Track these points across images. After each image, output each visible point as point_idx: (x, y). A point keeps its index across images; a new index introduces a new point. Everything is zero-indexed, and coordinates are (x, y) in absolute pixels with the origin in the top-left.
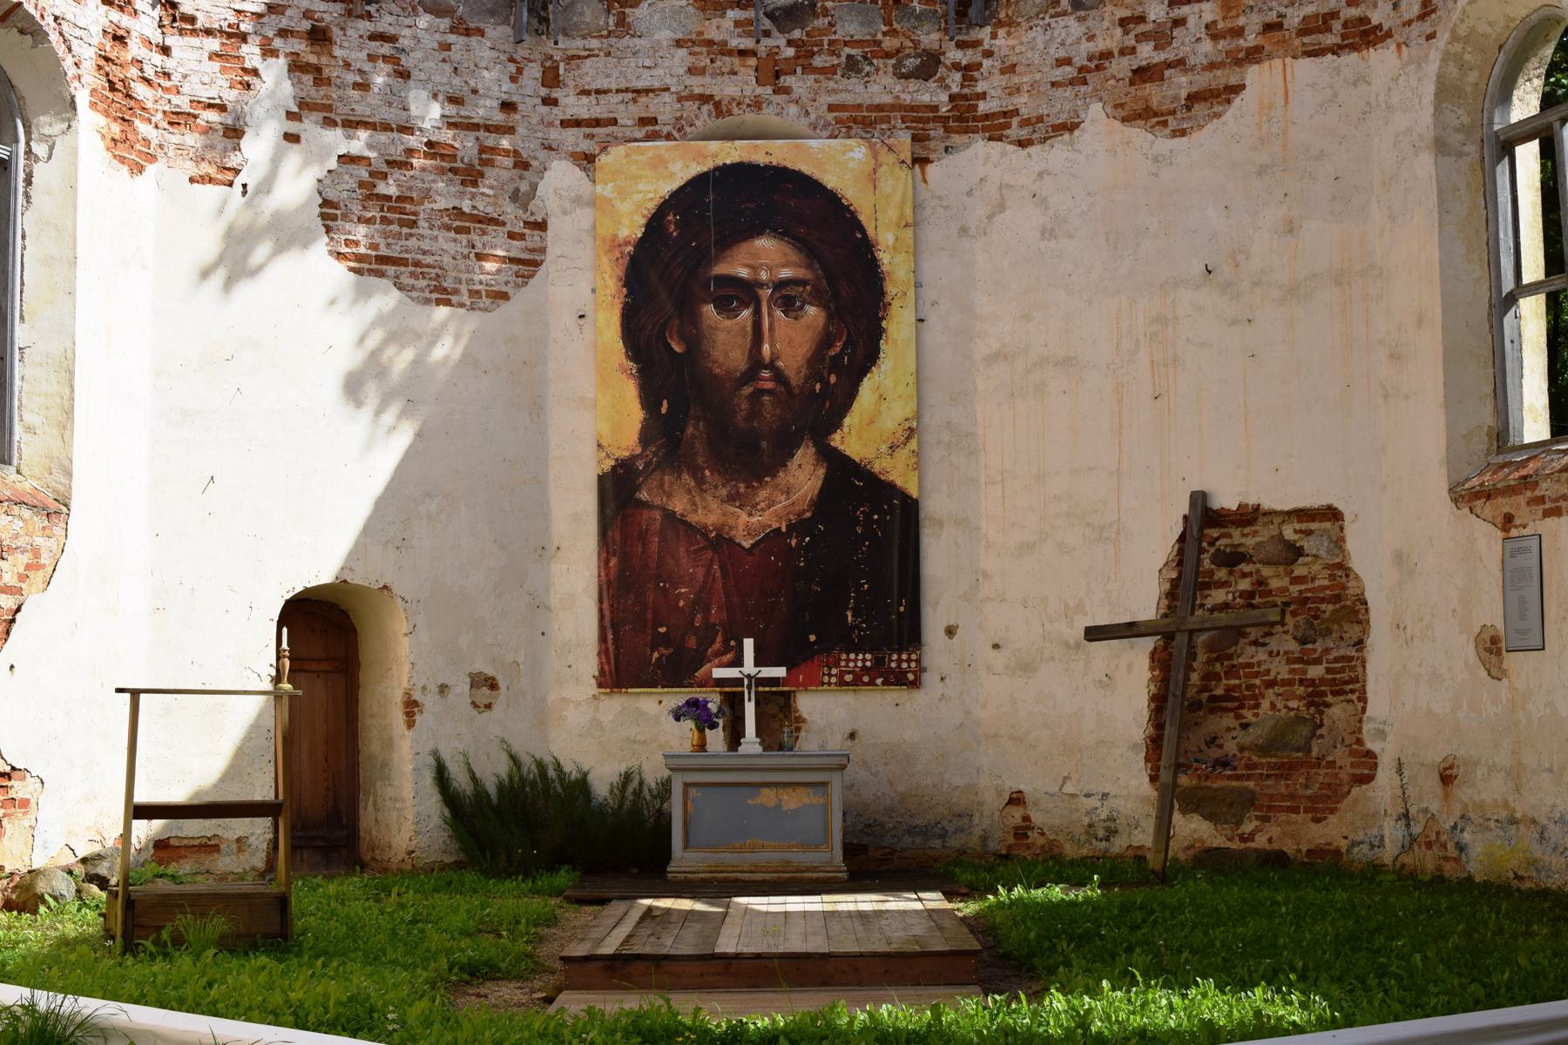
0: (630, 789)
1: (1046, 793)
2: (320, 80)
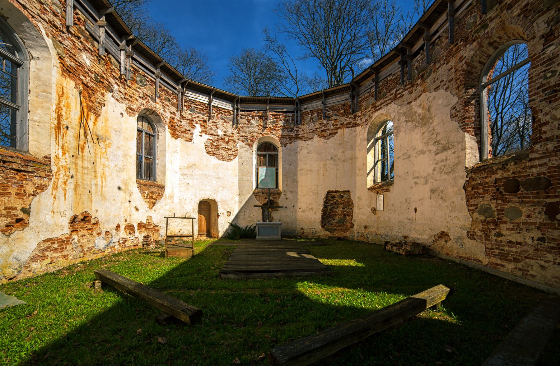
0: (248, 228)
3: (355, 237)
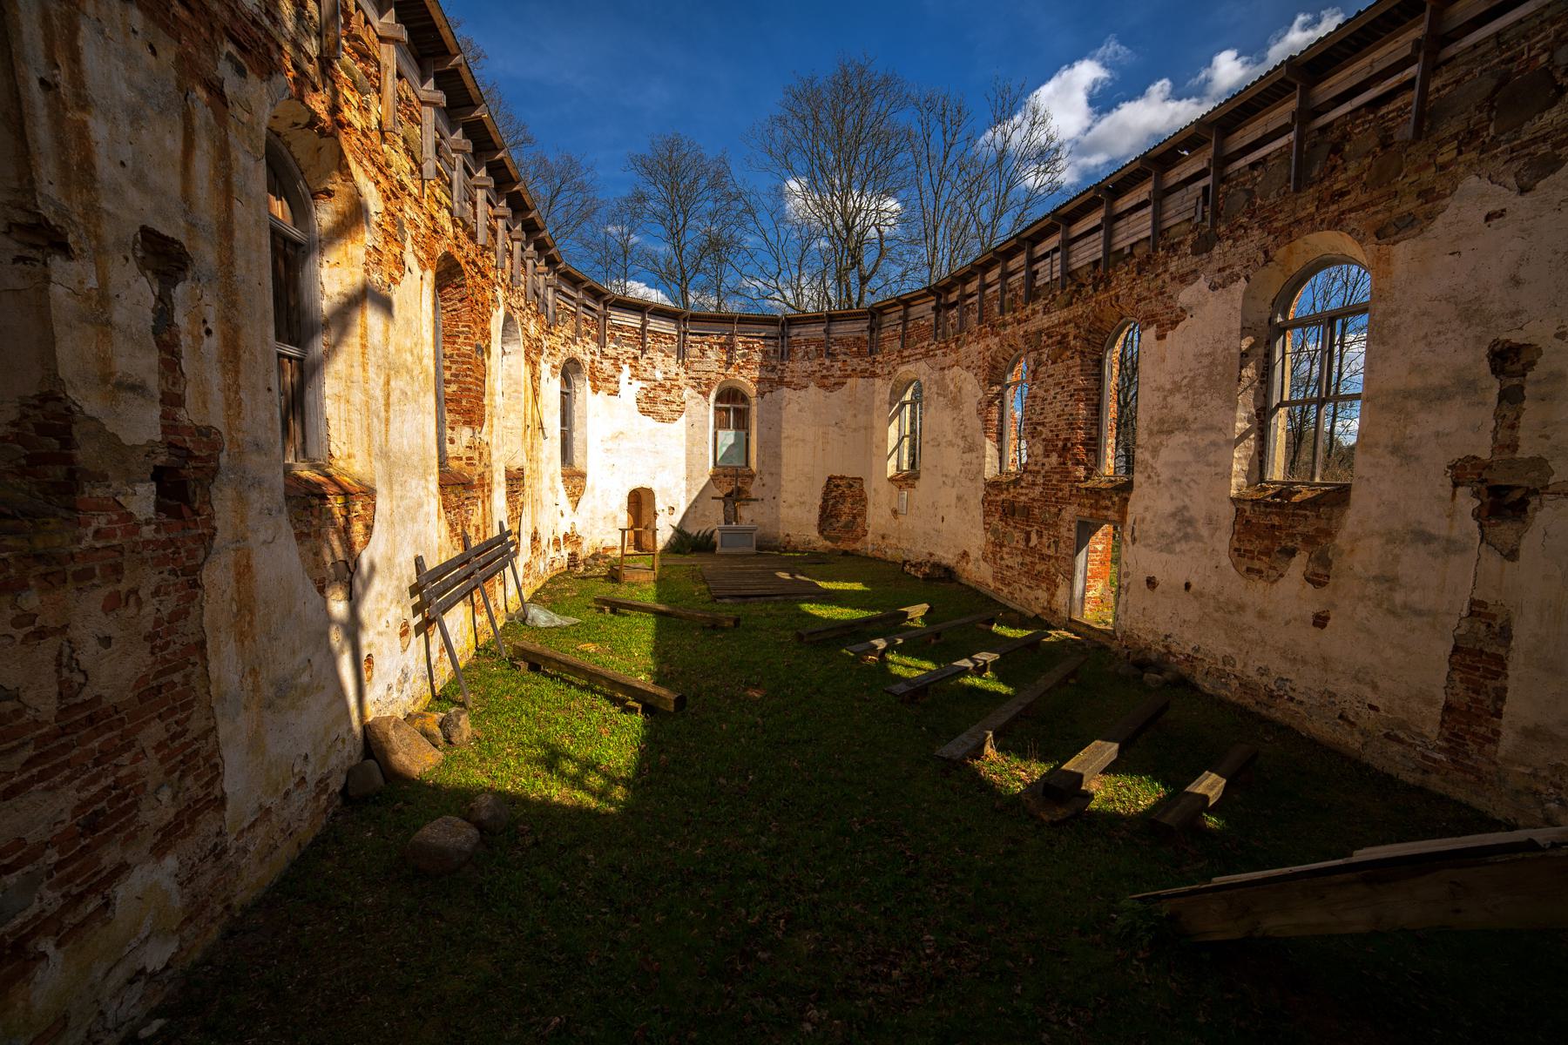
2: (636, 369)
3: (869, 551)
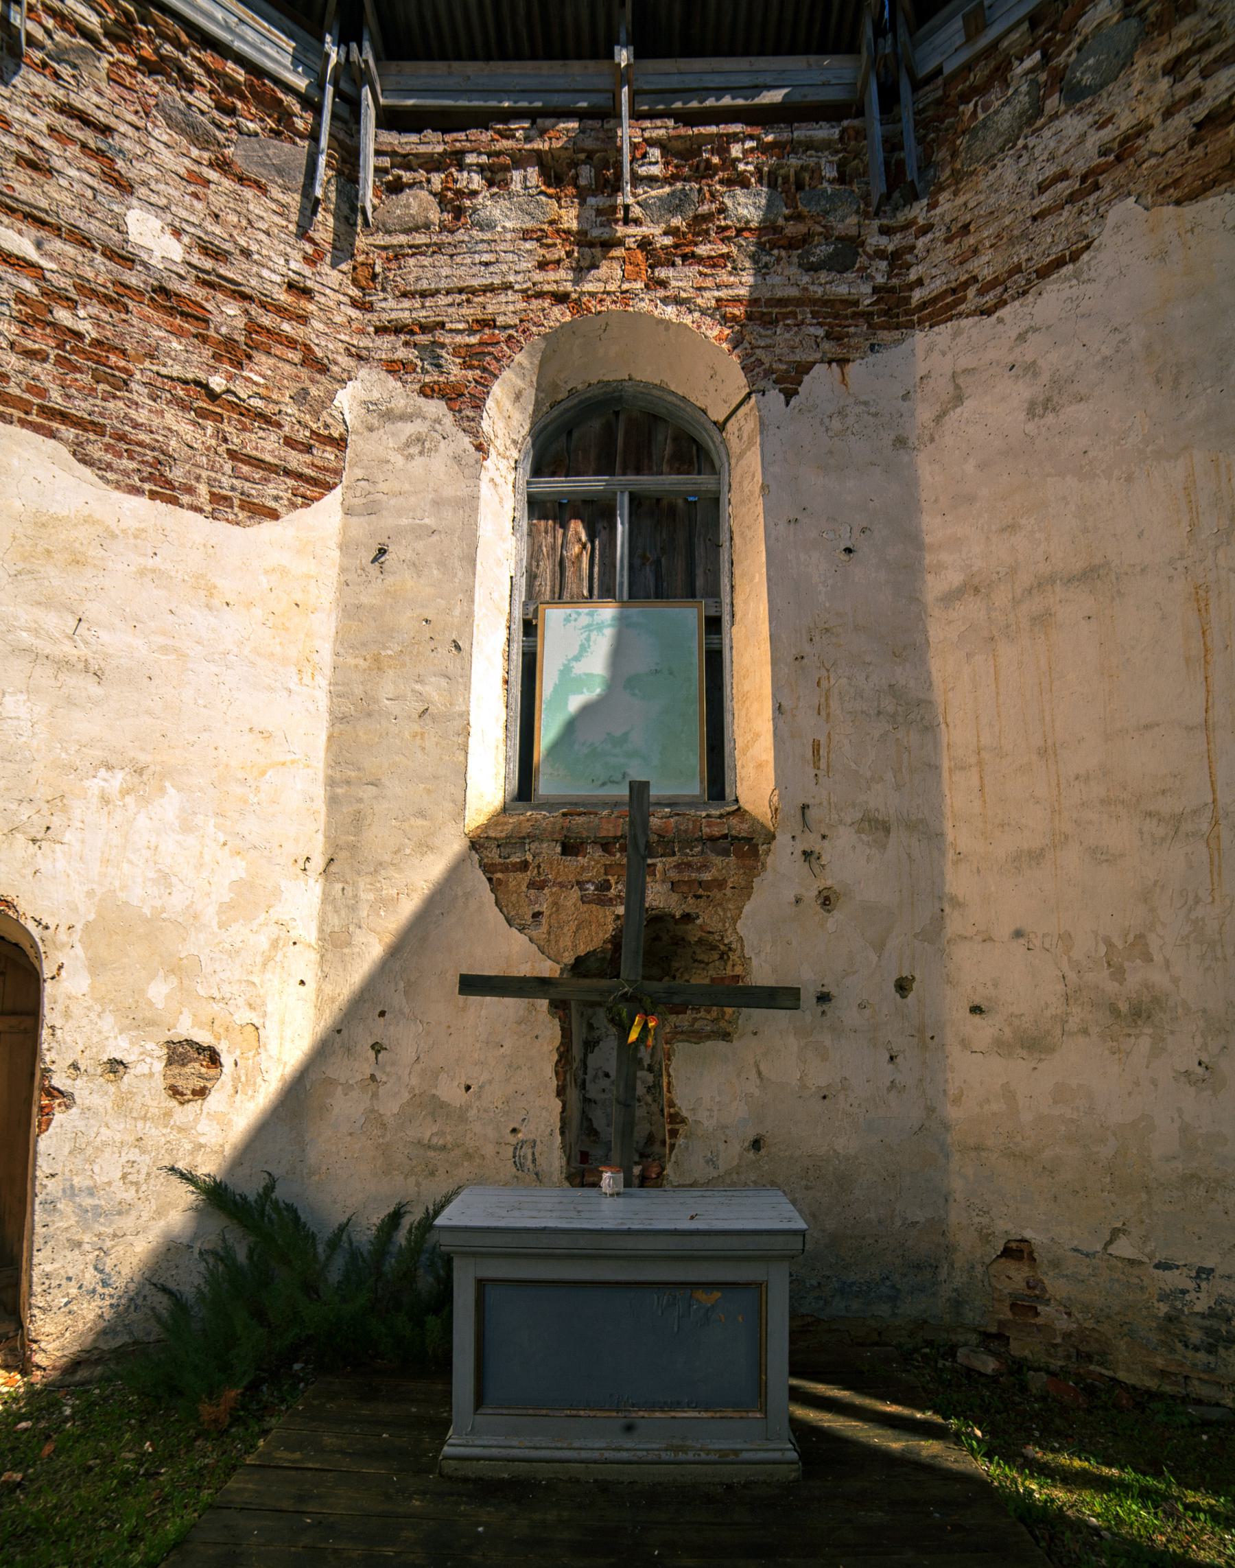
0: (401, 1237)
1: (1076, 1250)
